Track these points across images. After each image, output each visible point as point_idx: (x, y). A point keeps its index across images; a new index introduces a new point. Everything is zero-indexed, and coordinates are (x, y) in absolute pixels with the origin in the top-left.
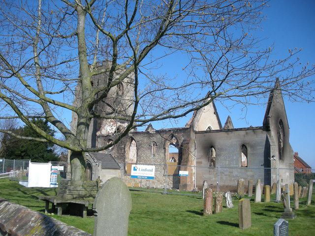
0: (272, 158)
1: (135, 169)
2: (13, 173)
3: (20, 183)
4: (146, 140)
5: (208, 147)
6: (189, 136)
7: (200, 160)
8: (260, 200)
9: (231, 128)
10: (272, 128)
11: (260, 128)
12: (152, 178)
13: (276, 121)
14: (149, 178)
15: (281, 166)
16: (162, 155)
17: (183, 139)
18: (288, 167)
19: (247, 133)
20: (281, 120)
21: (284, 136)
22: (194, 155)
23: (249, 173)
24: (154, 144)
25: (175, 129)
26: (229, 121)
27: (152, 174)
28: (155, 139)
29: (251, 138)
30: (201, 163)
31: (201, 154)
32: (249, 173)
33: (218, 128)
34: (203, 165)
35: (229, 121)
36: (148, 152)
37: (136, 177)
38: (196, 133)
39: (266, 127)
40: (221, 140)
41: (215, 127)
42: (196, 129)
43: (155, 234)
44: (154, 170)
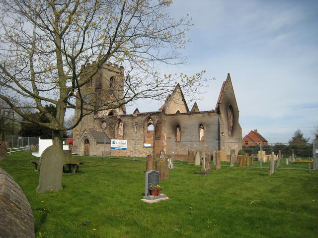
0: (221, 134)
1: (114, 143)
2: (27, 147)
3: (33, 154)
4: (130, 121)
5: (176, 126)
6: (161, 117)
7: (170, 136)
8: (199, 164)
9: (197, 111)
10: (222, 111)
11: (213, 111)
12: (125, 149)
13: (226, 106)
14: (123, 149)
15: (231, 140)
16: (142, 132)
17: (157, 120)
18: (237, 141)
19: (203, 115)
20: (231, 105)
21: (233, 117)
22: (166, 132)
23: (206, 146)
24: (136, 124)
25: (151, 112)
26: (195, 106)
27: (125, 146)
28: (136, 120)
29: (207, 119)
30: (170, 138)
31: (171, 131)
32: (206, 146)
33: (186, 112)
34: (171, 140)
35: (195, 106)
36: (131, 131)
37: (114, 148)
38: (167, 115)
39: (218, 111)
40: (185, 121)
41: (183, 110)
42: (167, 113)
43: (248, 236)
44: (126, 143)
